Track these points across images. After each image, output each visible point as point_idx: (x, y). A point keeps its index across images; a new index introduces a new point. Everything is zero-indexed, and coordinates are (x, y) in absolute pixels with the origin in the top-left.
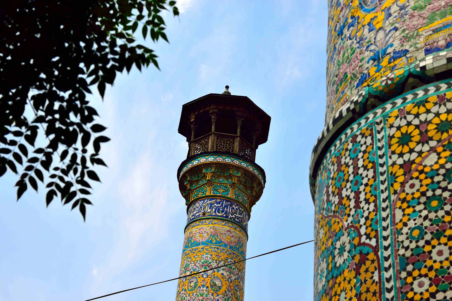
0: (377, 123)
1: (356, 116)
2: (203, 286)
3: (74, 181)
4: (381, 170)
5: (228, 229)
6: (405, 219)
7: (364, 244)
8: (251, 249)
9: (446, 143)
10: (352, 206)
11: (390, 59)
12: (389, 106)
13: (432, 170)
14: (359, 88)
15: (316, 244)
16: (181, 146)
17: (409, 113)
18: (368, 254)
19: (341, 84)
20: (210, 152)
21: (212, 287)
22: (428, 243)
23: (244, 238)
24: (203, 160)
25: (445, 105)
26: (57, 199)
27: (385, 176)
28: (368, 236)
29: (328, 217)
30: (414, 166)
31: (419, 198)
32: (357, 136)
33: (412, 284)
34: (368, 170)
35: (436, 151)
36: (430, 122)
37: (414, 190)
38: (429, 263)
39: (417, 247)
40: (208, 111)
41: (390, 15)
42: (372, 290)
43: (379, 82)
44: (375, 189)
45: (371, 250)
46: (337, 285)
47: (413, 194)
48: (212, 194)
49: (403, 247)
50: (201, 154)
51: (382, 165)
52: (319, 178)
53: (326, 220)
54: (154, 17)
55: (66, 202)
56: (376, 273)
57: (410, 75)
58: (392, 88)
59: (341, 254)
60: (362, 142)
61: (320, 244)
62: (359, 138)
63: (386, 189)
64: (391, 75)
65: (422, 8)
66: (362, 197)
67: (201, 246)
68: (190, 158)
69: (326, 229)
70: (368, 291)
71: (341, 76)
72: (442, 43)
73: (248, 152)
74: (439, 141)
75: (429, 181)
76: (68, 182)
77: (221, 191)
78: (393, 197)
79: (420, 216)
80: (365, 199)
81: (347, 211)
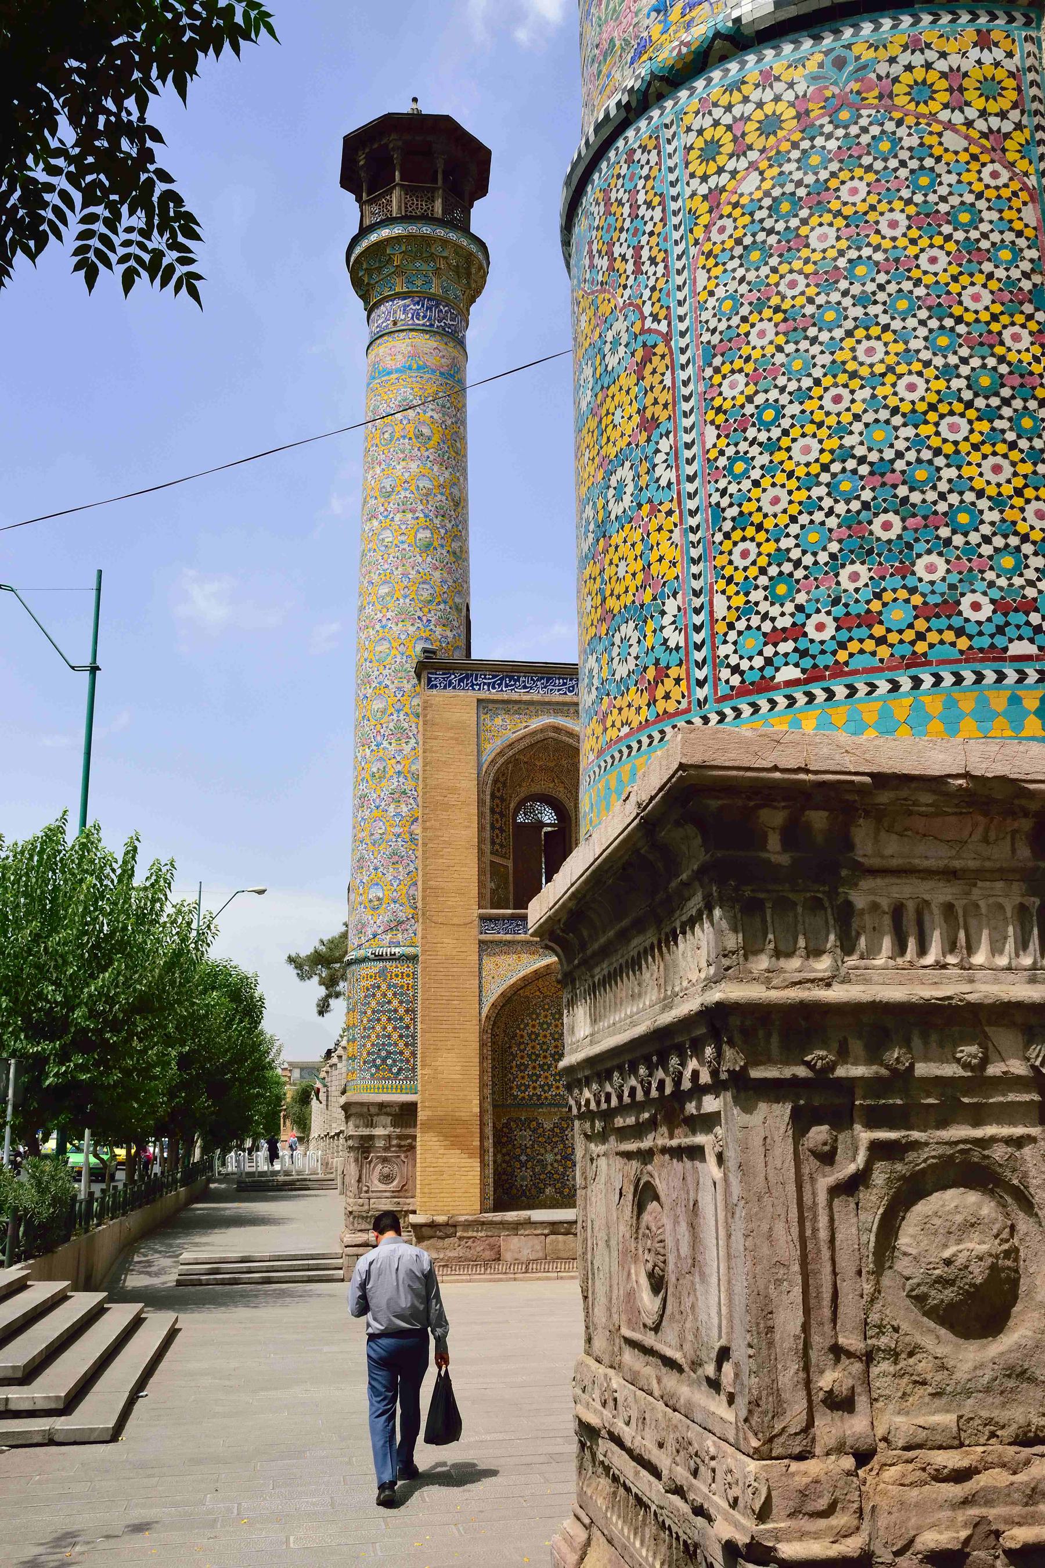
0: (666, 126)
1: (631, 115)
2: (404, 437)
3: (163, 247)
4: (674, 206)
6: (711, 286)
9: (773, 153)
10: (629, 272)
11: (684, 8)
12: (683, 94)
13: (752, 200)
14: (635, 65)
16: (347, 211)
17: (715, 105)
18: (655, 346)
19: (605, 60)
20: (396, 218)
21: (417, 437)
22: (744, 319)
24: (385, 233)
25: (771, 87)
26: (143, 280)
28: (655, 318)
29: (593, 293)
30: (725, 195)
32: (634, 151)
33: (720, 385)
34: (653, 208)
35: (757, 169)
36: (749, 119)
37: (725, 236)
38: (746, 351)
39: (729, 327)
40: (386, 145)
42: (662, 401)
43: (668, 52)
44: (665, 240)
46: (609, 400)
48: (405, 290)
49: (708, 329)
50: (382, 221)
51: (675, 199)
52: (576, 230)
53: (591, 297)
56: (668, 373)
57: (718, 35)
59: (614, 351)
61: (581, 339)
63: (682, 238)
64: (686, 37)
66: (645, 254)
67: (394, 376)
68: (364, 231)
70: (656, 402)
71: (605, 45)
74: (762, 151)
76: (154, 250)
77: (419, 283)
78: (693, 251)
79: (734, 278)
80: (650, 258)
81: (622, 281)
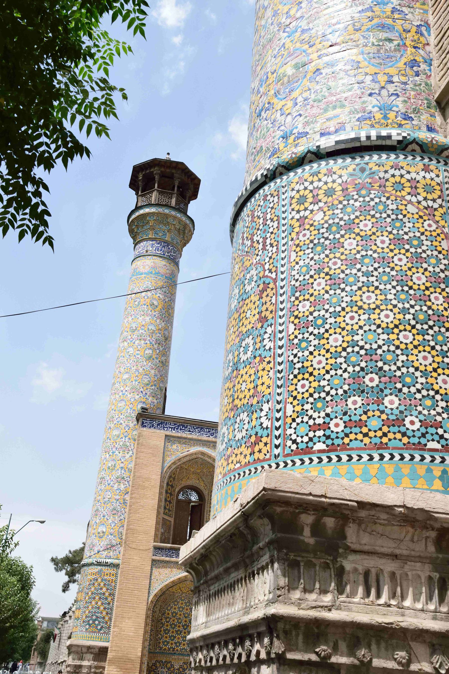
0: (283, 187)
4: (283, 222)
5: (165, 263)
6: (297, 260)
7: (267, 276)
8: (181, 278)
15: (232, 275)
16: (130, 198)
17: (306, 180)
22: (312, 277)
23: (176, 271)
24: (147, 210)
25: (331, 176)
27: (286, 227)
28: (270, 271)
30: (307, 220)
31: (308, 244)
37: (305, 238)
38: (311, 291)
39: (304, 279)
40: (153, 172)
41: (296, 104)
42: (270, 309)
43: (286, 156)
44: (278, 236)
45: (271, 281)
47: (304, 241)
50: (146, 205)
51: (284, 219)
54: (107, 99)
55: (37, 240)
56: (274, 297)
58: (295, 160)
59: (249, 284)
60: (271, 201)
62: (269, 197)
64: (295, 151)
65: (320, 101)
66: (268, 241)
67: (144, 276)
68: (137, 208)
69: (240, 264)
70: (267, 310)
72: (332, 129)
73: (182, 206)
74: (325, 203)
75: (316, 232)
77: (160, 234)
78: (290, 243)
80: (270, 244)
